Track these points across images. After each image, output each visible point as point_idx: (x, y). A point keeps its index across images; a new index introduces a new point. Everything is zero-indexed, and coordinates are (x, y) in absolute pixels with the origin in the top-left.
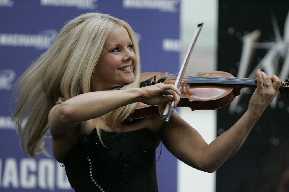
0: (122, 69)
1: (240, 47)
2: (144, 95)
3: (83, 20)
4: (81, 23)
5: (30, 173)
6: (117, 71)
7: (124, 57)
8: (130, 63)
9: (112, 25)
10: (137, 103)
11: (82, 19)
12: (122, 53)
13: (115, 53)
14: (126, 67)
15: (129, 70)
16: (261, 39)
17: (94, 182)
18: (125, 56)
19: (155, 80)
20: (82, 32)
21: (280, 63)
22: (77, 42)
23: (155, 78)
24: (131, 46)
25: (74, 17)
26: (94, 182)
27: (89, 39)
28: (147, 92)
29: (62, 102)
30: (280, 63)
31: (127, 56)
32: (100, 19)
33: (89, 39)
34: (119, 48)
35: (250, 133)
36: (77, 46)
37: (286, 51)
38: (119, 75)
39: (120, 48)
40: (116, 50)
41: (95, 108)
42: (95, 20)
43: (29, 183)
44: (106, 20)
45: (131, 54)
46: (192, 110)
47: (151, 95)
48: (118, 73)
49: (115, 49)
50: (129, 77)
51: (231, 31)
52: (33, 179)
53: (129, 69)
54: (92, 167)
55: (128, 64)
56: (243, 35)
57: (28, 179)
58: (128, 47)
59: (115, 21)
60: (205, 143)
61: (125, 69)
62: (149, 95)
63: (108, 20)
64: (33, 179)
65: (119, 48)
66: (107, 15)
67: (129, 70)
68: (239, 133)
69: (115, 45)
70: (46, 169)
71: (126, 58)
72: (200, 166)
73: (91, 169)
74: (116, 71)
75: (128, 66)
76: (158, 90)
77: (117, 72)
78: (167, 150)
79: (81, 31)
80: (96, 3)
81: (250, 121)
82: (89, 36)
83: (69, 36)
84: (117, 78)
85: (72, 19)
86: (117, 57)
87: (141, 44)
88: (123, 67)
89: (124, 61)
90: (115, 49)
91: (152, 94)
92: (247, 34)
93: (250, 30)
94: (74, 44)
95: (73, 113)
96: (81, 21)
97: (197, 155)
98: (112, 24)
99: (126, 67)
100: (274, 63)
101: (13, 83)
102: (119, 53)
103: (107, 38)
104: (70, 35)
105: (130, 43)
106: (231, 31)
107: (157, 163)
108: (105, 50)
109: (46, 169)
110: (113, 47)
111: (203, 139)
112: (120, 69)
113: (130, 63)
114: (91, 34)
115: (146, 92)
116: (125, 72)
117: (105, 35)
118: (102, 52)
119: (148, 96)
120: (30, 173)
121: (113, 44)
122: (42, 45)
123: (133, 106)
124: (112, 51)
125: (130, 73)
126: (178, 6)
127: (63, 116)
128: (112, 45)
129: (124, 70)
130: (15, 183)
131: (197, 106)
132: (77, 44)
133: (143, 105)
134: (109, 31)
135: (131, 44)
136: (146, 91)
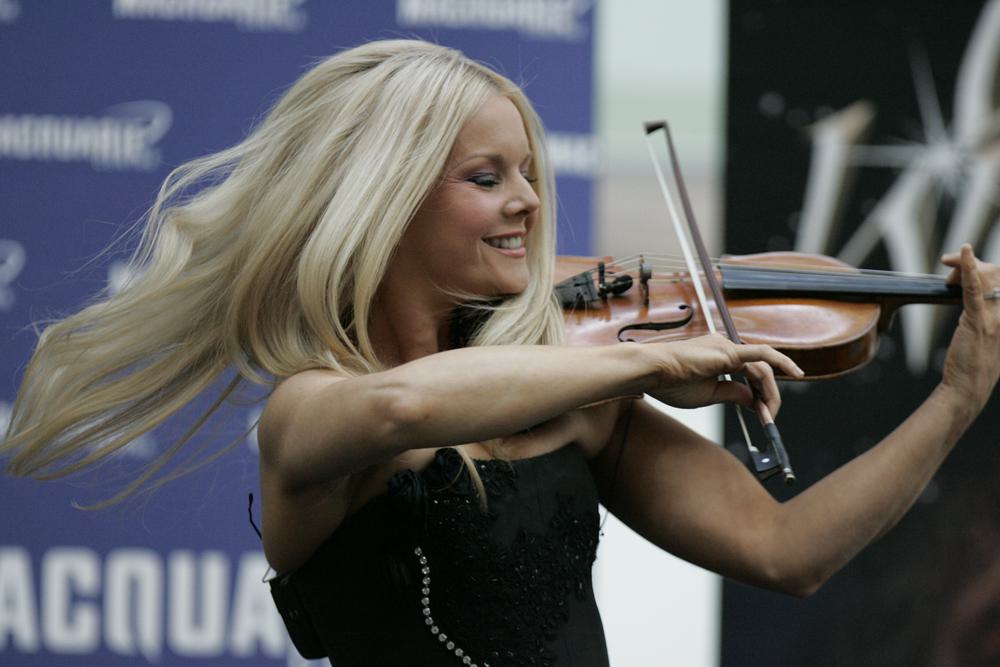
0: (496, 242)
1: (800, 161)
2: (668, 370)
3: (377, 60)
4: (369, 68)
5: (75, 597)
6: (482, 248)
7: (507, 203)
11: (372, 55)
14: (508, 237)
15: (516, 248)
16: (874, 135)
18: (513, 199)
21: (941, 214)
22: (358, 133)
25: (345, 45)
27: (406, 127)
28: (680, 363)
29: (105, 297)
31: (520, 199)
33: (406, 127)
36: (359, 147)
38: (486, 261)
43: (73, 634)
47: (693, 374)
50: (510, 273)
51: (771, 104)
52: (86, 620)
56: (813, 119)
57: (70, 619)
59: (488, 77)
61: (506, 243)
62: (684, 372)
64: (86, 620)
67: (516, 248)
69: (486, 156)
70: (134, 587)
71: (516, 206)
74: (478, 246)
75: (515, 235)
76: (720, 361)
79: (372, 97)
82: (405, 114)
83: (322, 109)
84: (478, 273)
85: (333, 52)
86: (488, 203)
88: (501, 238)
89: (507, 216)
91: (696, 371)
92: (825, 115)
94: (347, 136)
95: (427, 417)
96: (371, 63)
99: (508, 237)
103: (462, 129)
104: (331, 108)
106: (771, 104)
107: (268, 565)
108: (449, 169)
109: (134, 587)
112: (489, 241)
114: (411, 112)
115: (675, 363)
116: (506, 256)
117: (456, 119)
118: (440, 178)
119: (682, 375)
120: (75, 598)
121: (478, 153)
122: (117, 154)
125: (518, 260)
127: (388, 426)
128: (476, 156)
129: (500, 247)
130: (26, 636)
132: (357, 139)
134: (470, 105)
136: (677, 357)
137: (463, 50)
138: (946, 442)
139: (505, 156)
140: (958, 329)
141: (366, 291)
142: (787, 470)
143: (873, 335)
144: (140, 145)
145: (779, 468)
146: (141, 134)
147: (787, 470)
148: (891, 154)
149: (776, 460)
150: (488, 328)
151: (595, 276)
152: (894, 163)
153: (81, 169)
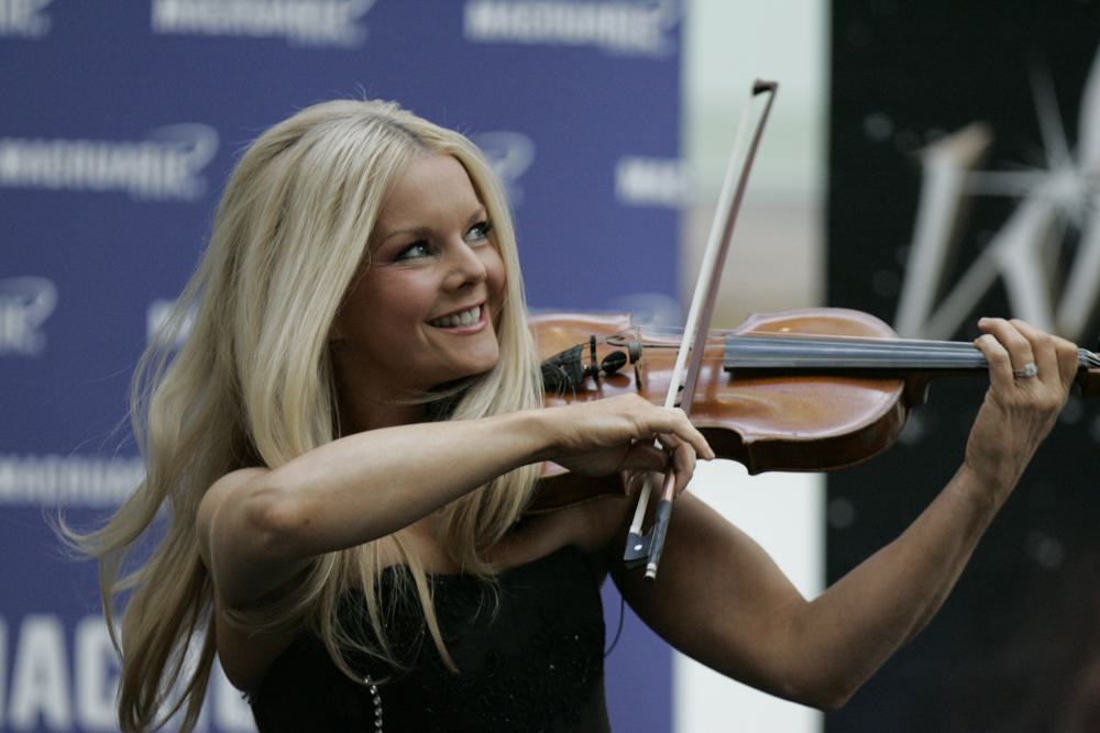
3: (295, 135)
6: (423, 333)
7: (446, 277)
8: (480, 294)
9: (398, 153)
10: (540, 464)
12: (442, 260)
13: (411, 262)
16: (994, 159)
17: (377, 718)
18: (452, 273)
19: (594, 358)
20: (288, 192)
21: (1064, 249)
23: (593, 350)
24: (484, 228)
26: (377, 718)
30: (1064, 249)
31: (460, 270)
32: (353, 130)
34: (429, 242)
35: (975, 552)
37: (1088, 205)
38: (434, 345)
39: (431, 243)
40: (415, 252)
41: (391, 497)
42: (337, 134)
44: (377, 134)
45: (480, 260)
46: (752, 472)
48: (429, 339)
49: (410, 247)
50: (481, 348)
51: (878, 126)
53: (472, 319)
54: (382, 705)
55: (467, 302)
56: (924, 142)
58: (465, 238)
60: (802, 600)
63: (384, 133)
65: (429, 242)
66: (387, 109)
68: (935, 559)
69: (410, 232)
71: (457, 279)
72: (788, 688)
73: (372, 692)
75: (469, 309)
77: (426, 335)
78: (647, 628)
80: (367, 20)
81: (978, 504)
83: (253, 202)
84: (425, 359)
85: (256, 135)
86: (422, 279)
87: (520, 215)
88: (450, 315)
89: (448, 292)
90: (410, 247)
92: (937, 139)
93: (951, 125)
95: (307, 522)
97: (777, 649)
98: (399, 150)
99: (459, 313)
100: (1042, 251)
101: (214, 174)
102: (430, 259)
105: (476, 215)
106: (878, 126)
110: (399, 241)
111: (786, 580)
112: (436, 322)
113: (480, 294)
118: (363, 263)
122: (157, 181)
123: (528, 474)
124: (401, 255)
125: (475, 337)
126: (675, 32)
127: (265, 537)
128: (396, 233)
131: (764, 457)
133: (555, 469)
135: (479, 221)
137: (399, 101)
138: (970, 531)
139: (434, 226)
140: (984, 405)
141: (301, 377)
142: (652, 566)
143: (901, 411)
144: (183, 173)
145: (645, 559)
146: (184, 160)
147: (652, 566)
148: (1011, 181)
149: (647, 550)
150: (252, 435)
151: (586, 353)
152: (1013, 192)
153: (117, 201)
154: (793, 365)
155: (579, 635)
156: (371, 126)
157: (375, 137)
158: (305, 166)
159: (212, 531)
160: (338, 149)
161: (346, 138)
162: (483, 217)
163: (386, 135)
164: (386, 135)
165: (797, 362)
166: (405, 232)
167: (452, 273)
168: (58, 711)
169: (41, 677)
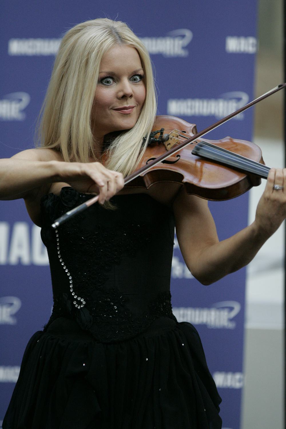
39: (115, 78)
44: (105, 34)
66: (119, 26)
69: (106, 73)
85: (72, 26)
154: (213, 159)
155: (117, 312)
156: (105, 31)
157: (104, 34)
158: (80, 41)
159: (195, 150)
160: (91, 36)
161: (95, 33)
162: (141, 72)
163: (109, 35)
164: (109, 35)
165: (214, 158)
166: (104, 72)
167: (120, 91)
168: (26, 260)
169: (20, 246)
